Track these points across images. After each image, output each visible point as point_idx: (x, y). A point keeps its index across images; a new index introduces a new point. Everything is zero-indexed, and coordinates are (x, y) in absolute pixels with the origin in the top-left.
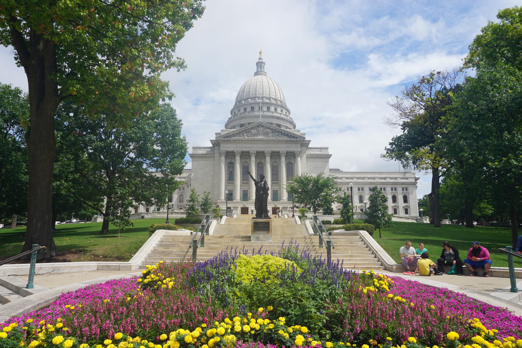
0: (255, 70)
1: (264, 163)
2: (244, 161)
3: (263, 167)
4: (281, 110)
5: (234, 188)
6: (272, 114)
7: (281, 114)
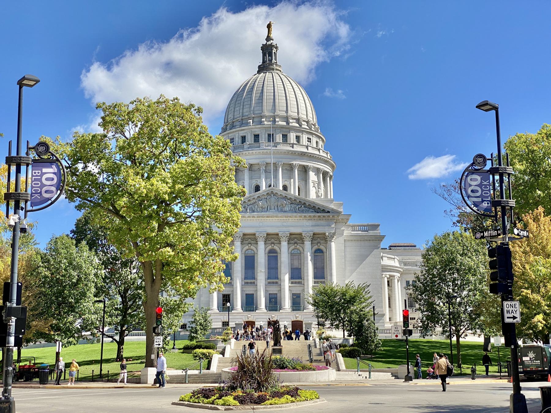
0: (260, 62)
1: (279, 251)
2: (247, 247)
3: (277, 256)
4: (308, 138)
5: (233, 291)
6: (291, 149)
7: (307, 147)
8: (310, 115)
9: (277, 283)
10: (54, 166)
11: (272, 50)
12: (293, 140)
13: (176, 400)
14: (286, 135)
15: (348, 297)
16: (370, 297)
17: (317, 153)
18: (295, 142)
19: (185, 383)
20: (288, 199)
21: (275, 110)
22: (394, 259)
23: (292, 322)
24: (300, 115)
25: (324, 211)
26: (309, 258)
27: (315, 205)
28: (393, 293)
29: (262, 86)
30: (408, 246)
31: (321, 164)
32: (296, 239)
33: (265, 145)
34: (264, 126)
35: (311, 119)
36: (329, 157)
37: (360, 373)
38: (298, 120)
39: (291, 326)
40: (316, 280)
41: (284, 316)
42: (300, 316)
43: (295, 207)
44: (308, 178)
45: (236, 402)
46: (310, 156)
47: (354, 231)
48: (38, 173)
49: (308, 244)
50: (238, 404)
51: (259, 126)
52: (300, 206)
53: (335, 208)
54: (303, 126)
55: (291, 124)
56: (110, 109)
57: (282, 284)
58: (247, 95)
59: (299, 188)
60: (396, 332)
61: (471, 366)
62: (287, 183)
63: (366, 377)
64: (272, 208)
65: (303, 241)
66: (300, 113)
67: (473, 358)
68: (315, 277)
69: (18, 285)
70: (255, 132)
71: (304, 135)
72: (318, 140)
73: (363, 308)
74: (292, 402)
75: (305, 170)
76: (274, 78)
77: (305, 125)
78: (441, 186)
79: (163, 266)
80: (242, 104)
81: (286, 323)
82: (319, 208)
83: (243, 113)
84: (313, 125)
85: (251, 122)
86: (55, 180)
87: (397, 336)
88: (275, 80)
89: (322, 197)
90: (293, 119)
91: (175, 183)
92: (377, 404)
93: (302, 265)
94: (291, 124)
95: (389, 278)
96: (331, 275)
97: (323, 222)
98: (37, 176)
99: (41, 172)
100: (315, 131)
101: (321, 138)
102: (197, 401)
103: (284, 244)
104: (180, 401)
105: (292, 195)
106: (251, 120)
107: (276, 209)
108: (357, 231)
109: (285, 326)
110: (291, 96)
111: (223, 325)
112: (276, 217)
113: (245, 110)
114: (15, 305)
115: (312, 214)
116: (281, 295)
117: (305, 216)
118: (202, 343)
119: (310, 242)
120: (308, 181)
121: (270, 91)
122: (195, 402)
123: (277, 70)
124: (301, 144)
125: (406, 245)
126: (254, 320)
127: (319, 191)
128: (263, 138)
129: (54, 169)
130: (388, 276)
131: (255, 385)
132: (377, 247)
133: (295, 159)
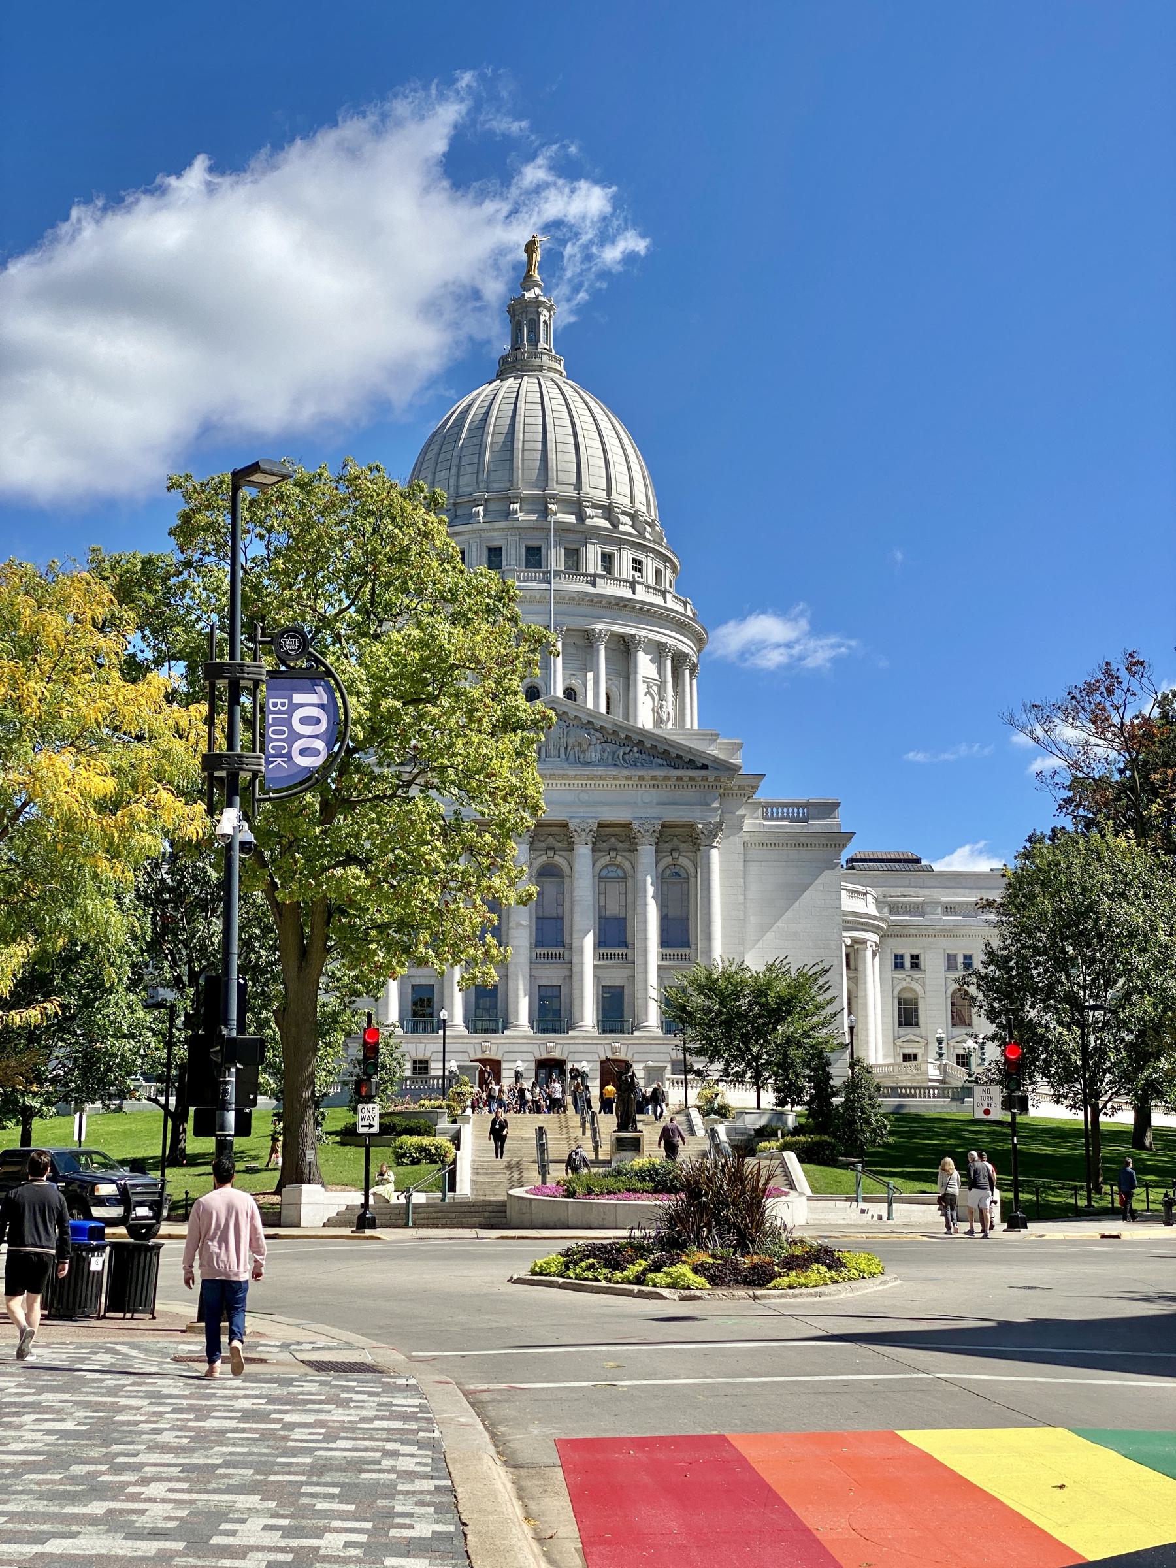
4: (635, 561)
6: (589, 589)
7: (632, 585)
8: (640, 497)
9: (560, 956)
10: (320, 689)
11: (539, 314)
12: (596, 565)
13: (524, 1274)
14: (577, 551)
15: (771, 998)
16: (831, 1001)
17: (658, 600)
18: (600, 571)
19: (406, 1226)
20: (596, 730)
21: (546, 480)
22: (865, 894)
23: (602, 1062)
24: (614, 495)
25: (692, 765)
26: (651, 890)
27: (668, 748)
28: (861, 986)
29: (510, 413)
30: (899, 861)
31: (668, 632)
32: (613, 839)
33: (519, 578)
34: (516, 524)
35: (644, 509)
36: (690, 614)
37: (863, 1205)
38: (608, 511)
39: (598, 1074)
40: (667, 951)
41: (581, 1048)
42: (623, 1048)
43: (614, 753)
44: (632, 670)
45: (701, 1280)
46: (641, 609)
47: (772, 819)
48: (283, 704)
49: (646, 853)
50: (708, 1286)
51: (503, 525)
52: (628, 749)
53: (721, 756)
54: (622, 528)
55: (588, 521)
56: (203, 491)
57: (575, 961)
58: (467, 438)
59: (608, 697)
60: (985, 1103)
61: (1164, 1191)
62: (575, 683)
63: (880, 1217)
64: (554, 752)
65: (632, 844)
66: (614, 492)
67: (1114, 1166)
68: (664, 943)
69: (239, 983)
70: (489, 540)
71: (624, 553)
72: (662, 567)
73: (812, 1029)
74: (835, 1282)
75: (625, 648)
76: (545, 392)
77: (626, 526)
78: (1025, 707)
79: (330, 915)
80: (455, 462)
81: (520, 1066)
82: (679, 756)
83: (457, 487)
84: (649, 524)
85: (481, 513)
86: (323, 726)
87: (987, 1112)
88: (546, 398)
89: (670, 725)
90: (594, 506)
91: (379, 694)
92: (1029, 1288)
93: (630, 906)
94: (588, 521)
95: (851, 946)
96: (709, 937)
97: (689, 794)
98: (280, 712)
99: (291, 700)
100: (654, 541)
101: (670, 560)
102: (590, 1274)
103: (583, 852)
104: (534, 1273)
105: (589, 713)
106: (481, 508)
107: (563, 755)
108: (777, 819)
109: (517, 1073)
110: (589, 443)
111: (415, 1068)
112: (563, 777)
113: (464, 480)
114: (234, 1034)
115: (660, 773)
116: (571, 989)
117: (641, 778)
118: (396, 1119)
119: (654, 848)
120: (632, 677)
121: (533, 429)
122: (586, 1279)
123: (551, 369)
124: (616, 575)
125: (893, 857)
126: (498, 1058)
127: (662, 706)
128: (513, 557)
129: (319, 696)
130: (849, 942)
131: (732, 1238)
132: (832, 865)
133: (599, 618)
